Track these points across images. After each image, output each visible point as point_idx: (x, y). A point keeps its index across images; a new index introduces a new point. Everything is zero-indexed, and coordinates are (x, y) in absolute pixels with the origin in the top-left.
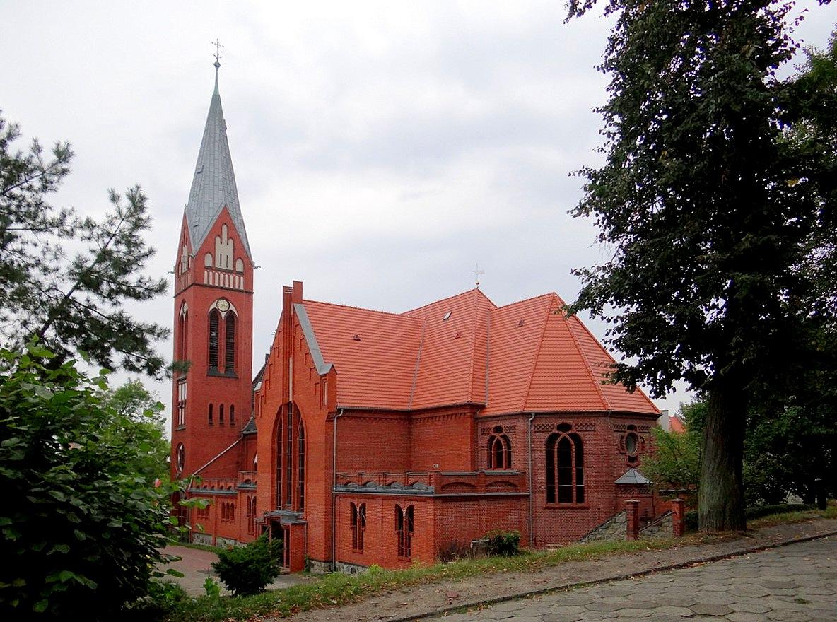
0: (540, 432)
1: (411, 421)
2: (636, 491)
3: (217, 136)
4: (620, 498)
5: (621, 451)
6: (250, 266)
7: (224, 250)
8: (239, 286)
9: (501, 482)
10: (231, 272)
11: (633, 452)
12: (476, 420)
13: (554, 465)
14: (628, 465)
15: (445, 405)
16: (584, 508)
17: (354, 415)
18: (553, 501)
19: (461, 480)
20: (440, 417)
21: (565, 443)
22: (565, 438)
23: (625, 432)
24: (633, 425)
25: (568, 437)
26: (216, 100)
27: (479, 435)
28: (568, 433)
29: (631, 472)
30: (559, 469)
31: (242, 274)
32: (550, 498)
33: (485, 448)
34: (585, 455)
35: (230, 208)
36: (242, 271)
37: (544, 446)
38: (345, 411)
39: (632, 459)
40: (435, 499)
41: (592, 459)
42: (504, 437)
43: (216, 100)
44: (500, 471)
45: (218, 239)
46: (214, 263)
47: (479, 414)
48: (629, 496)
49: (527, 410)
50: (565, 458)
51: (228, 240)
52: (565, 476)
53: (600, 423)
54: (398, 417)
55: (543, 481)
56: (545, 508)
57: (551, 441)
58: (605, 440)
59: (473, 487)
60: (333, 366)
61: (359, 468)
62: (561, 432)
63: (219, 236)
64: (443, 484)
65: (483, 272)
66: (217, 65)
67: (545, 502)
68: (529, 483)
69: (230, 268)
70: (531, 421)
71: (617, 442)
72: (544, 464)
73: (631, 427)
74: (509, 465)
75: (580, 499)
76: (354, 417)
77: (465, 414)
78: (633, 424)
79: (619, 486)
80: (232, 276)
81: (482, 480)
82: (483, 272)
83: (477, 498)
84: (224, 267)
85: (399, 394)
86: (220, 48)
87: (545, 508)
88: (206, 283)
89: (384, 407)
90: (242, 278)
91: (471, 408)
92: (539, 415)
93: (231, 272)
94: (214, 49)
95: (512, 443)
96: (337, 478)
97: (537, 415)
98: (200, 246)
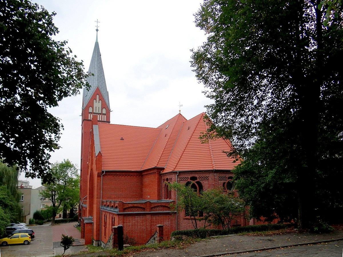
0: (182, 181)
1: (142, 176)
3: (96, 59)
6: (108, 111)
7: (97, 105)
8: (104, 120)
9: (161, 206)
10: (100, 114)
12: (160, 175)
15: (181, 171)
17: (112, 174)
19: (135, 205)
23: (226, 180)
25: (196, 184)
26: (97, 45)
28: (196, 181)
31: (105, 114)
32: (187, 214)
35: (100, 88)
36: (105, 113)
38: (106, 172)
40: (118, 215)
42: (199, 183)
43: (97, 45)
44: (168, 200)
45: (95, 101)
46: (93, 111)
47: (162, 172)
49: (176, 170)
51: (99, 100)
53: (211, 176)
54: (135, 174)
59: (144, 209)
60: (100, 152)
61: (115, 198)
63: (95, 99)
64: (152, 207)
65: (182, 105)
66: (97, 30)
69: (100, 112)
70: (178, 176)
76: (111, 175)
80: (101, 116)
81: (148, 205)
82: (182, 105)
84: (97, 112)
85: (119, 161)
86: (98, 23)
88: (89, 119)
89: (128, 169)
90: (105, 116)
91: (157, 170)
92: (180, 173)
93: (100, 114)
94: (96, 24)
96: (102, 202)
97: (180, 172)
98: (87, 104)
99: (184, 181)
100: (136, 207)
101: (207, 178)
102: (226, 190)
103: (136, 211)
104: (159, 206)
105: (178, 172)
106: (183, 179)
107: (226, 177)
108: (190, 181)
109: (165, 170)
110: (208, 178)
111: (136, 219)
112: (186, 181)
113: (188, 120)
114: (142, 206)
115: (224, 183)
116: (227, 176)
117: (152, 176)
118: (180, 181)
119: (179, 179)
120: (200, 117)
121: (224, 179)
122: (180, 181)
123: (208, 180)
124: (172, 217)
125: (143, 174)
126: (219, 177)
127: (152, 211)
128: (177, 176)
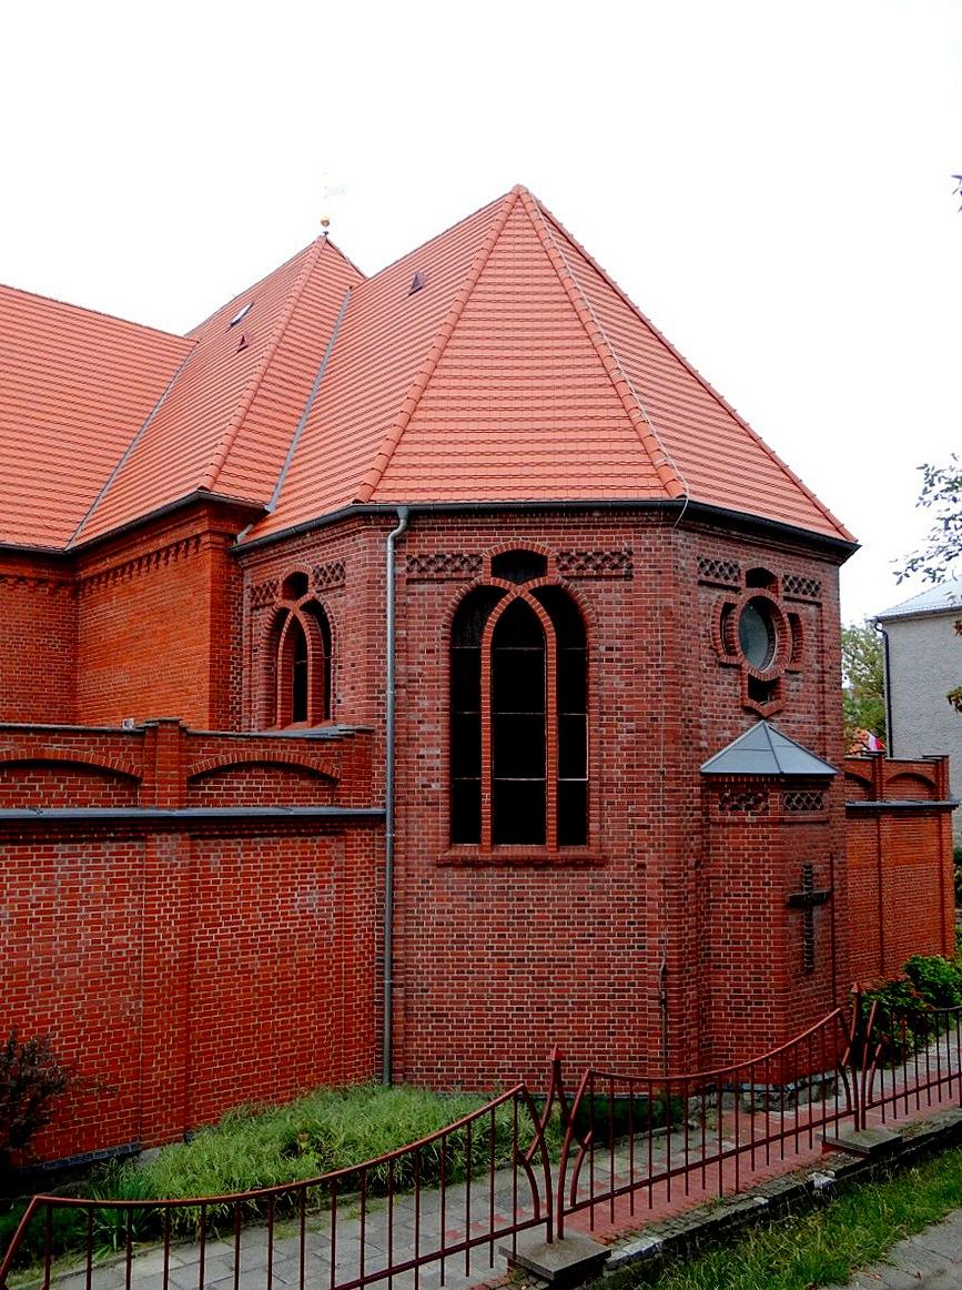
0: (431, 580)
1: (77, 589)
2: (775, 800)
4: (715, 824)
5: (725, 659)
9: (269, 766)
11: (761, 665)
12: (234, 559)
13: (477, 706)
14: (749, 710)
16: (587, 863)
18: (475, 837)
20: (140, 560)
21: (519, 622)
22: (518, 604)
23: (736, 590)
24: (761, 570)
27: (246, 611)
28: (536, 583)
29: (756, 733)
30: (495, 720)
32: (463, 826)
33: (261, 654)
34: (593, 668)
37: (441, 632)
39: (762, 690)
41: (618, 683)
44: (300, 730)
48: (749, 818)
50: (518, 680)
52: (519, 746)
53: (649, 544)
54: (28, 572)
55: (437, 763)
56: (442, 865)
57: (475, 604)
58: (668, 613)
59: (129, 782)
62: (502, 583)
67: (444, 840)
68: (383, 771)
70: (397, 542)
71: (710, 624)
72: (442, 701)
73: (759, 577)
74: (324, 713)
75: (574, 828)
77: (197, 537)
78: (766, 565)
79: (714, 782)
83: (137, 829)
87: (442, 865)
92: (422, 516)
95: (337, 628)
97: (418, 514)
99: (441, 581)
100: (291, 769)
101: (618, 566)
102: (734, 660)
103: (59, 803)
104: (249, 766)
105: (402, 513)
106: (439, 570)
107: (736, 566)
108: (492, 581)
109: (267, 524)
110: (631, 567)
111: (60, 867)
112: (460, 580)
113: (369, 273)
114: (117, 762)
115: (728, 607)
116: (741, 563)
117: (167, 572)
118: (409, 581)
119: (408, 570)
120: (506, 208)
121: (727, 578)
122: (409, 581)
123: (629, 577)
124: (357, 850)
125: (83, 575)
126: (702, 565)
127: (194, 803)
128: (390, 544)
